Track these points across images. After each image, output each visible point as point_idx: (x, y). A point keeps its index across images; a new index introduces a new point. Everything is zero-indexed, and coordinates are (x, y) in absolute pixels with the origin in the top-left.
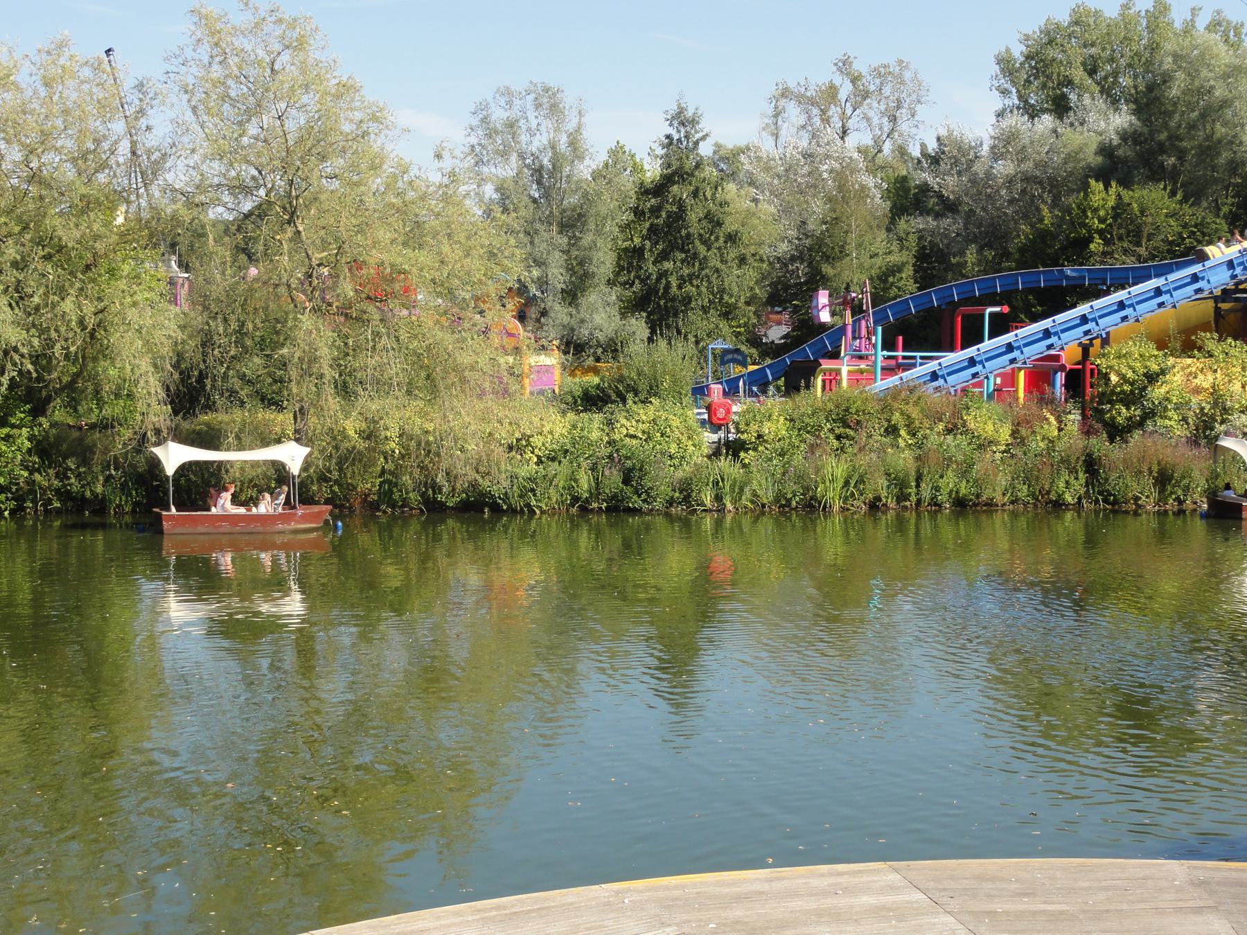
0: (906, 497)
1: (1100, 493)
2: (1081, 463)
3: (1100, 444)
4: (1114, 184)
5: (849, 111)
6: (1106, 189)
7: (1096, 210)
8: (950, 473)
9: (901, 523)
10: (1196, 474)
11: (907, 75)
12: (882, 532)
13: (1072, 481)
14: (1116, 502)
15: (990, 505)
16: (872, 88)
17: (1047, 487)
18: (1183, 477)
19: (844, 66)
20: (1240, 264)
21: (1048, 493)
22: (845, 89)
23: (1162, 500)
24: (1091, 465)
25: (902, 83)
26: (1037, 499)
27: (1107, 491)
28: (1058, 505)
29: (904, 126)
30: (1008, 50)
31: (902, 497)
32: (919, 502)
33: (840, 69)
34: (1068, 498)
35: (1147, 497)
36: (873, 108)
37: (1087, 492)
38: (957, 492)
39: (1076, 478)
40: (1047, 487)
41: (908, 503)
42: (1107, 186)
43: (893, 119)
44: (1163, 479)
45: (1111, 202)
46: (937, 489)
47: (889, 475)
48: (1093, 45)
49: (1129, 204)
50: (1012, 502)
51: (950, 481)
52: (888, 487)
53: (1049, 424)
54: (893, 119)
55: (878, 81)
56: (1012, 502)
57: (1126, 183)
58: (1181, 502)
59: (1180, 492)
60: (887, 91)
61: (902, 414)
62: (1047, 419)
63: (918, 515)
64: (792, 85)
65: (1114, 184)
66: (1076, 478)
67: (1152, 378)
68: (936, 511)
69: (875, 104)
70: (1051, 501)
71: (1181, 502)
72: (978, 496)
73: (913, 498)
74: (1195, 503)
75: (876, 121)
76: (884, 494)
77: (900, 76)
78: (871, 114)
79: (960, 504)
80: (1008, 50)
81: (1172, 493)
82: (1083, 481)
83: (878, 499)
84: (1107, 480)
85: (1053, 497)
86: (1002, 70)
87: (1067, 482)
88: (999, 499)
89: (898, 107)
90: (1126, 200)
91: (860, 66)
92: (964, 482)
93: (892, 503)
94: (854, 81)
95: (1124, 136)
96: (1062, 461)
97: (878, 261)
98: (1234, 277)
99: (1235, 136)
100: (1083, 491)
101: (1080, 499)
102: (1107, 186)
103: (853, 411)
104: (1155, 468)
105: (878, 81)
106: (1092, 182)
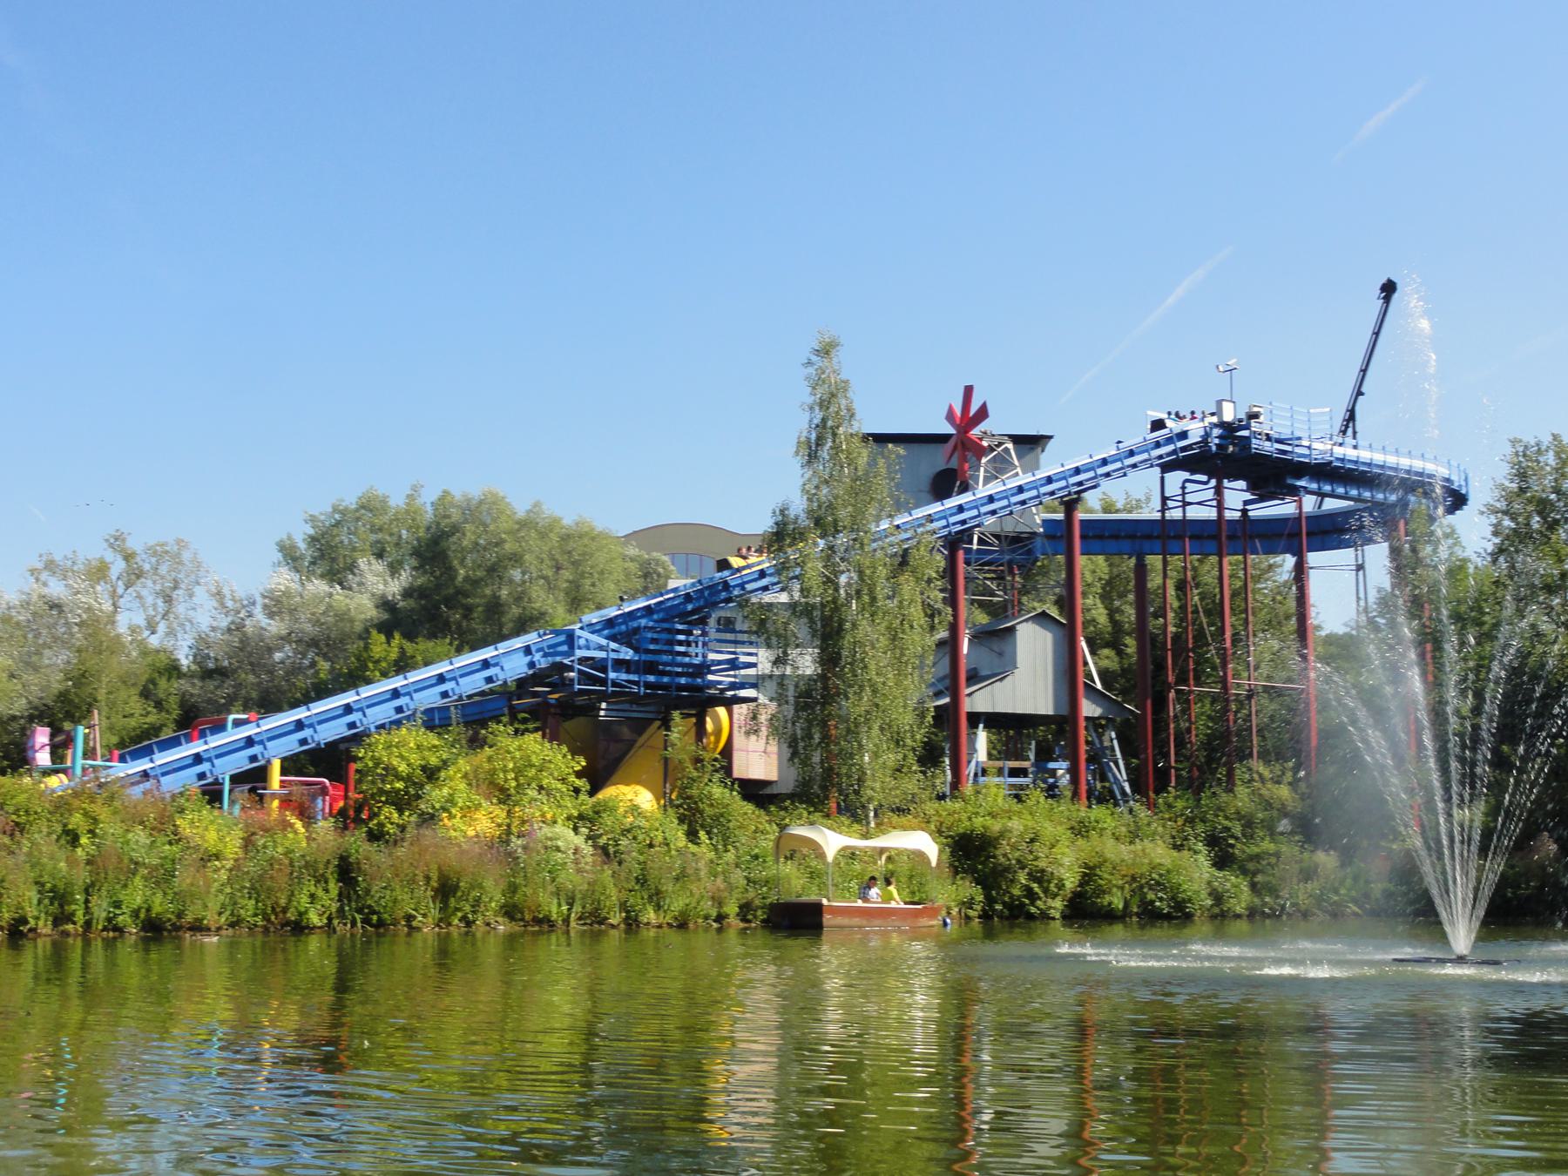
0: (69, 918)
1: (360, 911)
2: (331, 868)
3: (356, 842)
4: (397, 635)
5: (120, 591)
6: (388, 642)
7: (377, 662)
8: (138, 881)
9: (58, 954)
10: (489, 883)
11: (186, 556)
12: (26, 977)
13: (320, 893)
14: (381, 924)
15: (198, 927)
16: (147, 567)
17: (283, 902)
18: (472, 887)
19: (117, 542)
20: (538, 650)
21: (285, 910)
22: (118, 566)
23: (444, 921)
24: (346, 871)
25: (181, 563)
26: (269, 920)
27: (370, 907)
28: (299, 928)
29: (180, 609)
30: (289, 538)
31: (60, 919)
32: (88, 925)
33: (111, 546)
34: (314, 918)
35: (424, 916)
36: (147, 588)
37: (341, 911)
38: (148, 910)
39: (327, 891)
40: (283, 902)
41: (70, 927)
42: (389, 636)
43: (168, 600)
44: (446, 890)
45: (394, 655)
46: (117, 905)
47: (43, 885)
48: (380, 530)
49: (413, 657)
50: (232, 925)
51: (136, 895)
52: (40, 902)
53: (296, 832)
54: (168, 600)
55: (154, 560)
56: (232, 925)
57: (410, 636)
58: (469, 924)
59: (468, 908)
60: (163, 570)
61: (86, 814)
62: (291, 825)
63: (87, 943)
64: (58, 557)
65: (397, 635)
66: (327, 891)
67: (431, 774)
68: (115, 938)
69: (149, 583)
70: (288, 923)
71: (469, 924)
72: (180, 915)
73: (80, 916)
74: (488, 924)
75: (150, 600)
76: (31, 911)
77: (178, 555)
78: (144, 593)
79: (155, 930)
80: (289, 538)
81: (457, 909)
82: (334, 892)
83: (23, 920)
84: (367, 892)
85: (291, 915)
86: (285, 556)
87: (312, 896)
88: (211, 919)
89: (175, 588)
90: (410, 652)
91: (134, 544)
92: (159, 895)
93: (45, 927)
94: (128, 557)
95: (407, 593)
96: (307, 865)
97: (133, 722)
98: (532, 665)
99: (523, 592)
100: (335, 906)
101: (330, 919)
102: (389, 636)
103: (11, 809)
104: (434, 876)
105: (154, 560)
106: (374, 632)
